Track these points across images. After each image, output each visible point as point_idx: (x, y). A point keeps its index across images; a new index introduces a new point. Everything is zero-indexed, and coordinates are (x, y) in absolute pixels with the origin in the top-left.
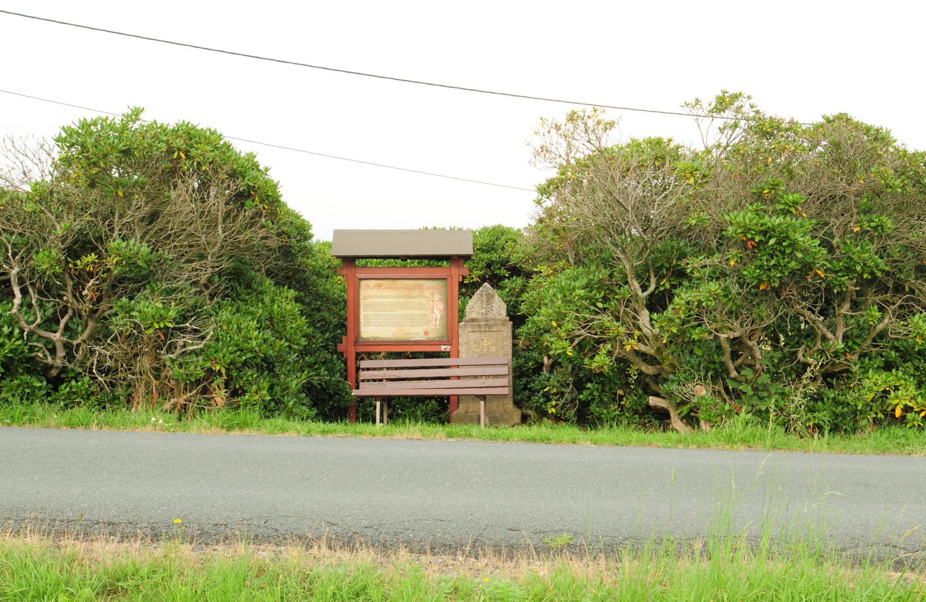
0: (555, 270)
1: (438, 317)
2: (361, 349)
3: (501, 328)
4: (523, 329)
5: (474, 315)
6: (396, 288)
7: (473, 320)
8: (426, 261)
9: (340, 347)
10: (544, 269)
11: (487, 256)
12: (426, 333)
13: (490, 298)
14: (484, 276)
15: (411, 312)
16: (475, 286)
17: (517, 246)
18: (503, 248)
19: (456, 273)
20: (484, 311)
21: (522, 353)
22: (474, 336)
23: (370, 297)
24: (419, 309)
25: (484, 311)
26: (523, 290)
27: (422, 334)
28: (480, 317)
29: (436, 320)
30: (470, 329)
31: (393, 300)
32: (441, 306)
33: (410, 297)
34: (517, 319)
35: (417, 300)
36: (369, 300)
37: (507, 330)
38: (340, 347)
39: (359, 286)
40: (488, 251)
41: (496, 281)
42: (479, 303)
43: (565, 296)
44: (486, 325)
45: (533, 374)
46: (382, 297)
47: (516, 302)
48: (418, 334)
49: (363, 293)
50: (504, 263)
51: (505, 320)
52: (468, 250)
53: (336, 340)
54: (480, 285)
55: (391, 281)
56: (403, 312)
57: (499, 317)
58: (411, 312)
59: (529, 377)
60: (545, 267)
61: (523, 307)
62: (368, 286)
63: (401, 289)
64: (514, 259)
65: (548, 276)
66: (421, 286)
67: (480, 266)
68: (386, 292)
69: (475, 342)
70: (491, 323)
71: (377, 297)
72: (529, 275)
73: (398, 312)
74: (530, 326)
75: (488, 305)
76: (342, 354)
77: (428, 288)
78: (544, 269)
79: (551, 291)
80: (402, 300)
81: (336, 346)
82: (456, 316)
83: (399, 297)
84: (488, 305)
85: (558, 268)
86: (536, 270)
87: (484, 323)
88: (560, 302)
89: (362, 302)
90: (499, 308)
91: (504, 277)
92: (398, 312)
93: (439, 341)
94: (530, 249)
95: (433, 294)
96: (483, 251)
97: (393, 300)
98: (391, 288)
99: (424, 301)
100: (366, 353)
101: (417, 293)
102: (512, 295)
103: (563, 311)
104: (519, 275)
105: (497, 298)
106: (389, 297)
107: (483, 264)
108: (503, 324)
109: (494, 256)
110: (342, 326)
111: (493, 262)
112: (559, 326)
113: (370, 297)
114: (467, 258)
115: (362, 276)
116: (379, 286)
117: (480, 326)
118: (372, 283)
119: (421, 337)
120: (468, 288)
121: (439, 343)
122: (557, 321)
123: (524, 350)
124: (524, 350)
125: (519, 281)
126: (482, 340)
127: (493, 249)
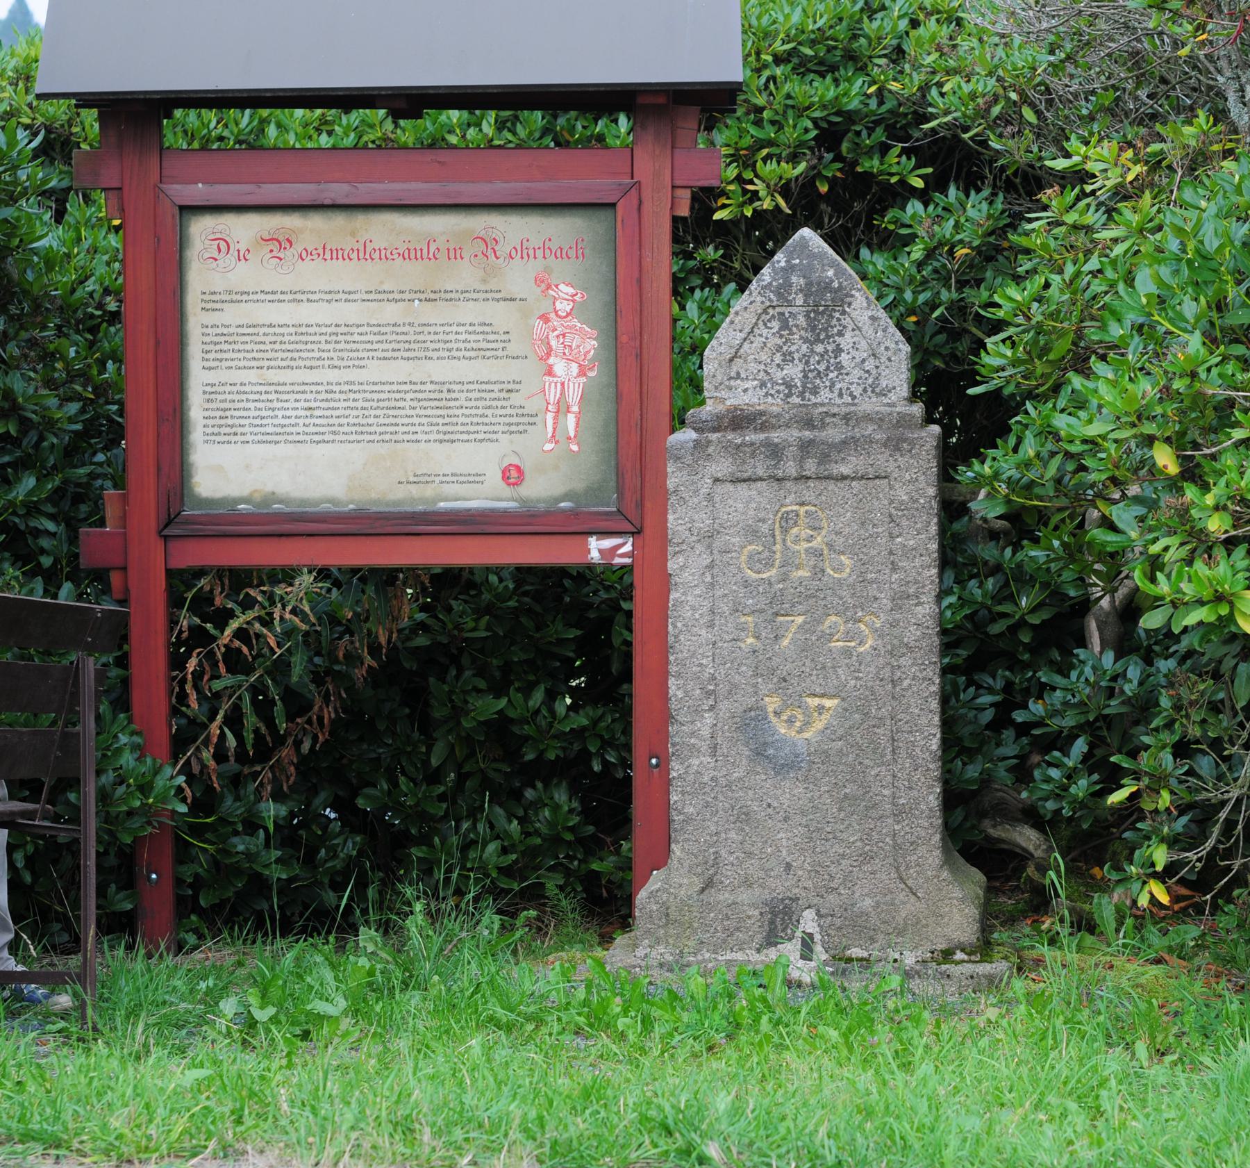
0: (1156, 163)
1: (573, 396)
2: (191, 555)
3: (883, 460)
4: (999, 463)
5: (745, 396)
6: (364, 253)
7: (739, 420)
8: (537, 118)
9: (95, 544)
10: (1104, 158)
11: (822, 90)
12: (514, 475)
13: (825, 308)
14: (808, 183)
15: (441, 370)
16: (766, 233)
17: (965, 44)
18: (898, 54)
19: (661, 177)
20: (794, 371)
21: (988, 552)
22: (743, 503)
23: (239, 296)
24: (481, 354)
25: (794, 371)
26: (996, 254)
27: (494, 476)
28: (774, 405)
29: (561, 408)
30: (722, 467)
31: (350, 313)
32: (588, 343)
33: (434, 296)
34: (960, 404)
35: (468, 312)
36: (232, 315)
37: (913, 477)
38: (95, 544)
39: (182, 243)
40: (825, 68)
41: (853, 212)
42: (769, 334)
43: (1220, 306)
44: (806, 447)
45: (1037, 648)
46: (296, 297)
47: (959, 308)
48: (476, 478)
49: (202, 277)
50: (902, 123)
51: (903, 421)
52: (725, 66)
53: (76, 504)
54: (791, 226)
55: (339, 221)
56: (398, 371)
57: (869, 405)
58: (441, 370)
59: (1014, 664)
60: (1107, 149)
61: (996, 355)
62: (223, 244)
63: (385, 255)
64: (950, 104)
65: (1122, 194)
66: (489, 244)
67: (790, 135)
68: (315, 274)
69: (752, 533)
70: (834, 433)
71: (272, 296)
72: (1026, 185)
73: (376, 371)
74: (1029, 448)
75: (818, 342)
76: (100, 576)
77: (522, 251)
78: (1104, 158)
79: (1145, 283)
80: (391, 313)
81: (73, 539)
82: (654, 391)
83: (379, 296)
84: (818, 342)
85: (1174, 156)
86: (1060, 164)
87: (795, 434)
88: (1195, 342)
89: (197, 322)
90: (874, 358)
91: (903, 193)
92: (376, 371)
93: (573, 514)
94: (1029, 57)
95: (544, 283)
96: (804, 68)
97: (350, 313)
98: (337, 254)
99: (501, 316)
100: (220, 572)
101: (465, 274)
102: (943, 277)
103: (1214, 389)
104: (970, 184)
105: (863, 308)
106: (331, 296)
107: (799, 130)
108: (895, 445)
109: (854, 92)
110: (104, 429)
111: (850, 117)
112: (1192, 473)
113: (239, 296)
114: (712, 102)
115: (198, 192)
116: (280, 242)
117: (775, 452)
118: (243, 228)
119: (487, 494)
120: (718, 248)
121: (574, 523)
122: (1176, 441)
123: (994, 535)
124: (994, 535)
125: (977, 211)
126: (788, 521)
127: (851, 57)
